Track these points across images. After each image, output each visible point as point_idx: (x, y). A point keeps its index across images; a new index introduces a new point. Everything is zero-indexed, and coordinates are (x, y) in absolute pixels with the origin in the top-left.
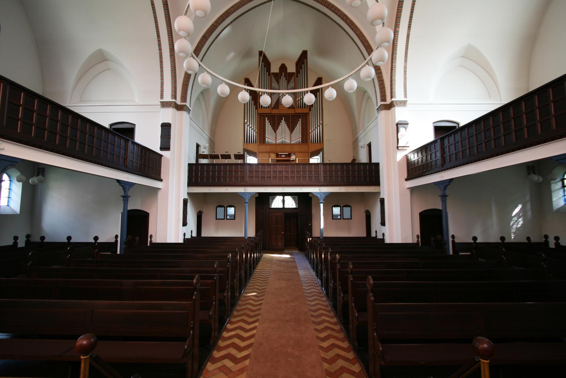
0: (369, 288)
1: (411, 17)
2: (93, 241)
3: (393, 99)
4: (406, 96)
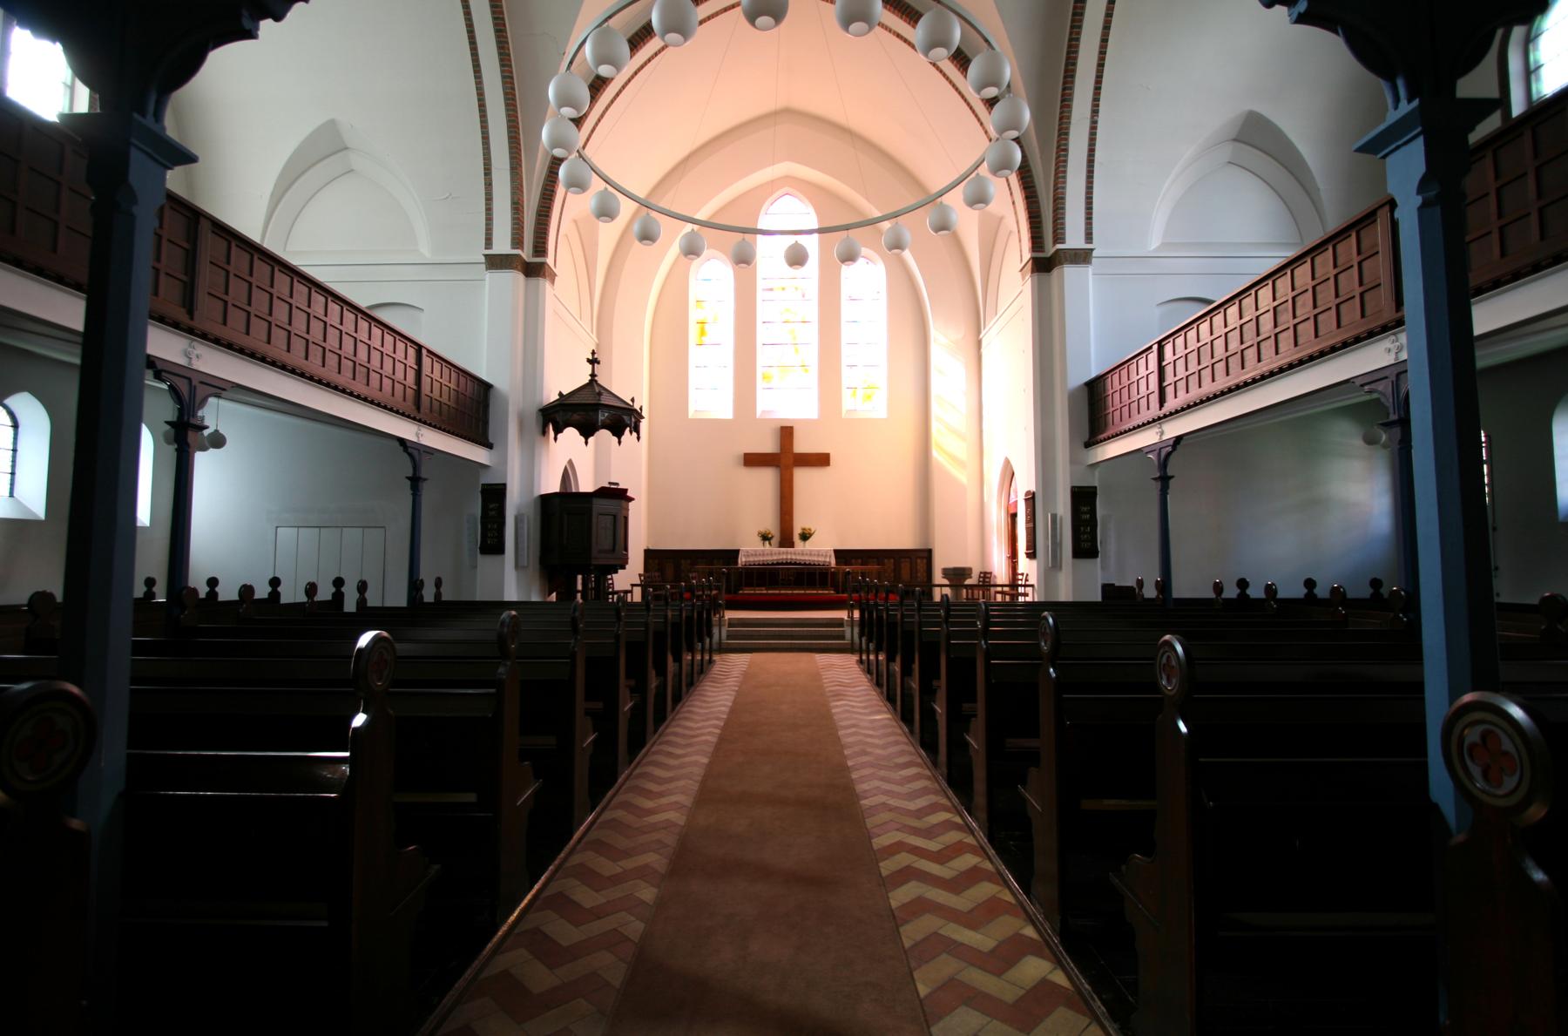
0: (1168, 685)
1: (1104, 41)
2: (1213, 595)
3: (1059, 246)
4: (1089, 237)
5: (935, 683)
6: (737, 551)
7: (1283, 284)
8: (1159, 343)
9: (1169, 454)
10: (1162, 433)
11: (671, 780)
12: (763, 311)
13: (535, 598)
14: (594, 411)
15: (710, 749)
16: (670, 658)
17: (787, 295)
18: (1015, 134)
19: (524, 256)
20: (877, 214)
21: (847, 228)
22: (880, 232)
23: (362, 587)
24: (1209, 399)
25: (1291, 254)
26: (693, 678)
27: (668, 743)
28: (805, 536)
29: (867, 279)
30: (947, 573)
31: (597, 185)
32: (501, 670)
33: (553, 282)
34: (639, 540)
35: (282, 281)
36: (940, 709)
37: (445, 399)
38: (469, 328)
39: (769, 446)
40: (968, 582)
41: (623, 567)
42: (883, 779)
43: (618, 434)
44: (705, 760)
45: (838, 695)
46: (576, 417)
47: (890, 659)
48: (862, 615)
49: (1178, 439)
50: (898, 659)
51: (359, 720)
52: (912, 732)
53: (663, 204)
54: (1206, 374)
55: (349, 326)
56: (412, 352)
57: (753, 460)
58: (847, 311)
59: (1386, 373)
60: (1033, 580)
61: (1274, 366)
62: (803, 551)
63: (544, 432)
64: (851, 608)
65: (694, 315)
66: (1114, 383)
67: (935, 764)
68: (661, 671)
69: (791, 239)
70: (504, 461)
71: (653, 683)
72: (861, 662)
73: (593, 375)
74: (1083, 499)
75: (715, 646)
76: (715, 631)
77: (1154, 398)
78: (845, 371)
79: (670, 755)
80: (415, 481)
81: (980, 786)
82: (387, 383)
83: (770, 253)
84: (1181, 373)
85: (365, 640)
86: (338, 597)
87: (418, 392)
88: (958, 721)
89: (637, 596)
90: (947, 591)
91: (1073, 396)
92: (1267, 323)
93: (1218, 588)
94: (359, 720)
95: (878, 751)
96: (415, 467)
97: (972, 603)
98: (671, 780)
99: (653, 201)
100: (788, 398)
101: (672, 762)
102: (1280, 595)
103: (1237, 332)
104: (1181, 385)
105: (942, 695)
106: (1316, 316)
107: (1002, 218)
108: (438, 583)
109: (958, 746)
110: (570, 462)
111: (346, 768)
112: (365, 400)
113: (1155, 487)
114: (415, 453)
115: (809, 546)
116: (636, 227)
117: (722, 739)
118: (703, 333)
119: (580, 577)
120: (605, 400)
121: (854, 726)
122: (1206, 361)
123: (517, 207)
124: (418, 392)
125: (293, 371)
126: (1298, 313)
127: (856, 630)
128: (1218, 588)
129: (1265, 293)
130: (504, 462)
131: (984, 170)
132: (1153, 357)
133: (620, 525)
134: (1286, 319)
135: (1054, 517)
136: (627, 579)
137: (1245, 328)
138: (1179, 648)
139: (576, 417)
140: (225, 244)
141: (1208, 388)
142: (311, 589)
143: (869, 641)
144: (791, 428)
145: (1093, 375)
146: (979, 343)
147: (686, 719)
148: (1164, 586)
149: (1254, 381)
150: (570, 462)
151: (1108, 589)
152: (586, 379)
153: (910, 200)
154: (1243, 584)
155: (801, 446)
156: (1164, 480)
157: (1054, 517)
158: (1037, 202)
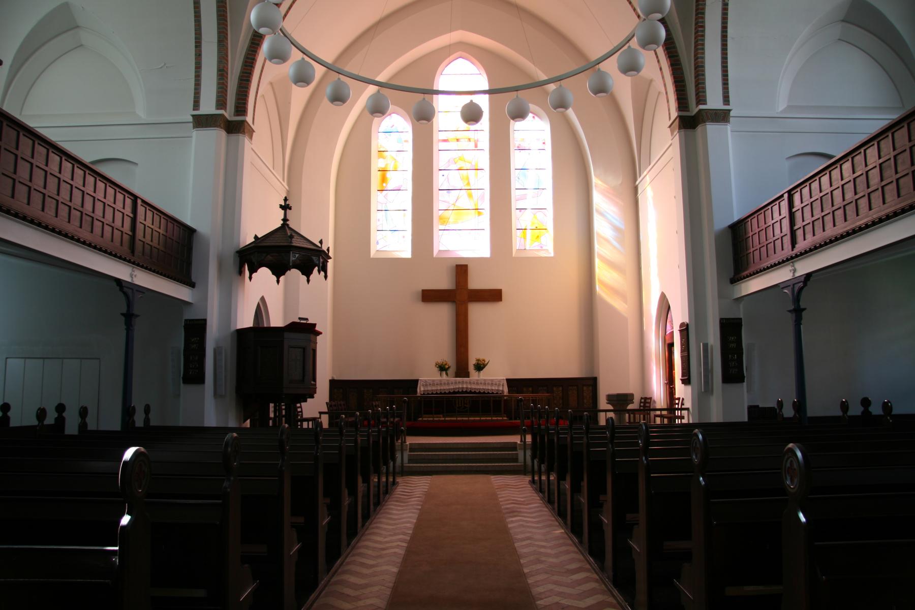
0: (791, 484)
2: (840, 413)
3: (702, 107)
4: (726, 99)
5: (602, 498)
6: (416, 381)
7: (886, 144)
8: (789, 192)
9: (801, 289)
10: (795, 271)
11: (366, 586)
12: (441, 159)
13: (232, 424)
14: (286, 252)
15: (400, 560)
16: (360, 479)
17: (462, 149)
18: (659, 16)
19: (227, 115)
20: (543, 77)
21: (516, 89)
22: (546, 93)
23: (83, 412)
24: (831, 242)
25: (895, 116)
26: (377, 500)
27: (360, 554)
28: (480, 367)
29: (533, 134)
30: (611, 399)
31: (296, 56)
32: (226, 484)
33: (251, 137)
34: (326, 370)
35: (25, 142)
36: (606, 520)
37: (155, 243)
38: (176, 179)
39: (444, 282)
40: (630, 407)
41: (313, 397)
42: (556, 583)
43: (307, 273)
44: (395, 570)
45: (513, 512)
46: (269, 258)
47: (561, 478)
48: (534, 439)
49: (808, 276)
50: (568, 478)
51: (126, 520)
52: (581, 542)
53: (348, 68)
54: (863, 203)
55: (54, 167)
56: (129, 202)
57: (430, 296)
58: (517, 159)
59: (788, 284)
60: (688, 404)
61: (882, 214)
62: (477, 380)
63: (241, 272)
64: (523, 433)
65: (377, 164)
66: (753, 226)
67: (602, 568)
68: (353, 492)
69: (466, 99)
70: (205, 298)
71: (346, 501)
72: (533, 482)
73: (285, 220)
74: (730, 329)
75: (397, 470)
76: (398, 455)
77: (787, 240)
78: (514, 174)
79: (363, 565)
80: (129, 317)
81: (641, 585)
82: (108, 229)
83: (447, 112)
84: (808, 219)
85: (129, 454)
86: (60, 421)
87: (133, 237)
88: (622, 528)
89: (325, 420)
90: (611, 415)
91: (719, 237)
92: (875, 175)
93: (844, 406)
94: (126, 520)
95: (551, 560)
96: (129, 305)
97: (634, 426)
98: (366, 586)
99: (339, 66)
100: (464, 238)
101: (365, 571)
102: (894, 412)
103: (852, 183)
104: (809, 229)
105: (608, 506)
106: (897, 180)
107: (651, 81)
108: (147, 410)
109: (622, 552)
110: (263, 299)
111: (116, 559)
112: (90, 245)
113: (790, 318)
114: (129, 292)
115: (484, 375)
116: (328, 90)
117: (409, 552)
118: (384, 179)
119: (272, 405)
120: (296, 242)
121: (528, 538)
122: (828, 209)
123: (222, 73)
124: (133, 237)
125: (32, 222)
126: (899, 169)
127: (529, 453)
128: (844, 406)
129: (872, 152)
130: (205, 299)
131: (634, 43)
132: (784, 204)
133: (309, 357)
134: (889, 173)
135: (706, 346)
136: (315, 407)
137: (858, 180)
138: (799, 454)
139: (269, 258)
140: (15, 133)
141: (831, 232)
142: (41, 414)
143: (541, 462)
144: (466, 266)
145: (736, 219)
146: (636, 189)
147: (374, 534)
148: (800, 406)
149: (867, 226)
150: (263, 299)
151: (752, 410)
152: (279, 223)
153: (573, 67)
154: (866, 402)
155: (476, 282)
156: (798, 312)
157: (706, 346)
158: (681, 69)
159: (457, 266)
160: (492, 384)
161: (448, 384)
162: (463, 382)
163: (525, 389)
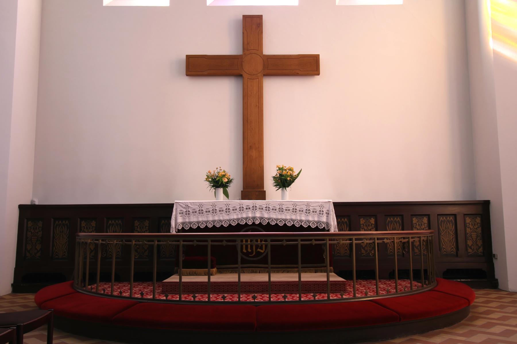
6: (170, 207)
28: (284, 181)
57: (200, 67)
62: (277, 206)
115: (293, 194)
144: (260, 17)
155: (276, 43)
159: (245, 17)
160: (308, 211)
161: (228, 210)
162: (254, 208)
163: (362, 221)
